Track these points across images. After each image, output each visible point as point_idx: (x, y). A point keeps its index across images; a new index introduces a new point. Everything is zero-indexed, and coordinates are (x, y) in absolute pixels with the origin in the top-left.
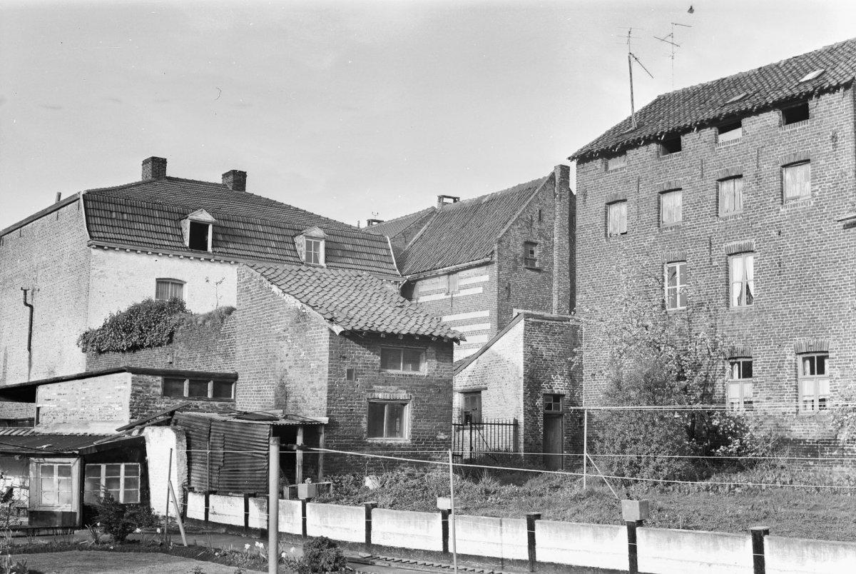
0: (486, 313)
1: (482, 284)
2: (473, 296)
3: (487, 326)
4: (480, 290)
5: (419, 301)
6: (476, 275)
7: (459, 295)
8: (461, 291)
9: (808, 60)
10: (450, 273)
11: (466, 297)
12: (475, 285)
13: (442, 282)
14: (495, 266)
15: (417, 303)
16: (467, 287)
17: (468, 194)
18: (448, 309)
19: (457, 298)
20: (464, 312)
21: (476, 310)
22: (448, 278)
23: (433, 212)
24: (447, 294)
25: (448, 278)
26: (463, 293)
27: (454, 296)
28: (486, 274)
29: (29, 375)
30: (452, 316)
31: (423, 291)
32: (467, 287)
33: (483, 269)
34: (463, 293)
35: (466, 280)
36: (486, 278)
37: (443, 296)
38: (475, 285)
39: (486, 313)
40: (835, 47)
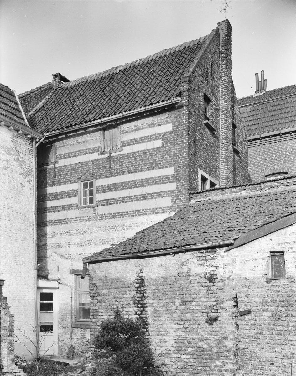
0: (170, 171)
1: (163, 136)
2: (145, 152)
3: (172, 186)
4: (158, 143)
5: (57, 165)
6: (152, 125)
7: (121, 153)
8: (124, 148)
9: (114, 83)
10: (106, 127)
11: (134, 155)
12: (149, 139)
13: (95, 139)
14: (184, 111)
15: (55, 168)
16: (135, 142)
17: (75, 75)
18: (104, 171)
19: (119, 158)
20: (130, 172)
21: (150, 169)
22: (104, 134)
23: (47, 88)
24: (102, 153)
25: (104, 134)
26: (127, 150)
27: (112, 155)
28: (167, 123)
29: (4, 97)
30: (111, 178)
31: (63, 152)
32: (135, 142)
33: (163, 117)
34: (127, 150)
35: (133, 133)
36: (169, 127)
37: (95, 156)
38: (149, 139)
39: (170, 171)
40: (201, 41)
